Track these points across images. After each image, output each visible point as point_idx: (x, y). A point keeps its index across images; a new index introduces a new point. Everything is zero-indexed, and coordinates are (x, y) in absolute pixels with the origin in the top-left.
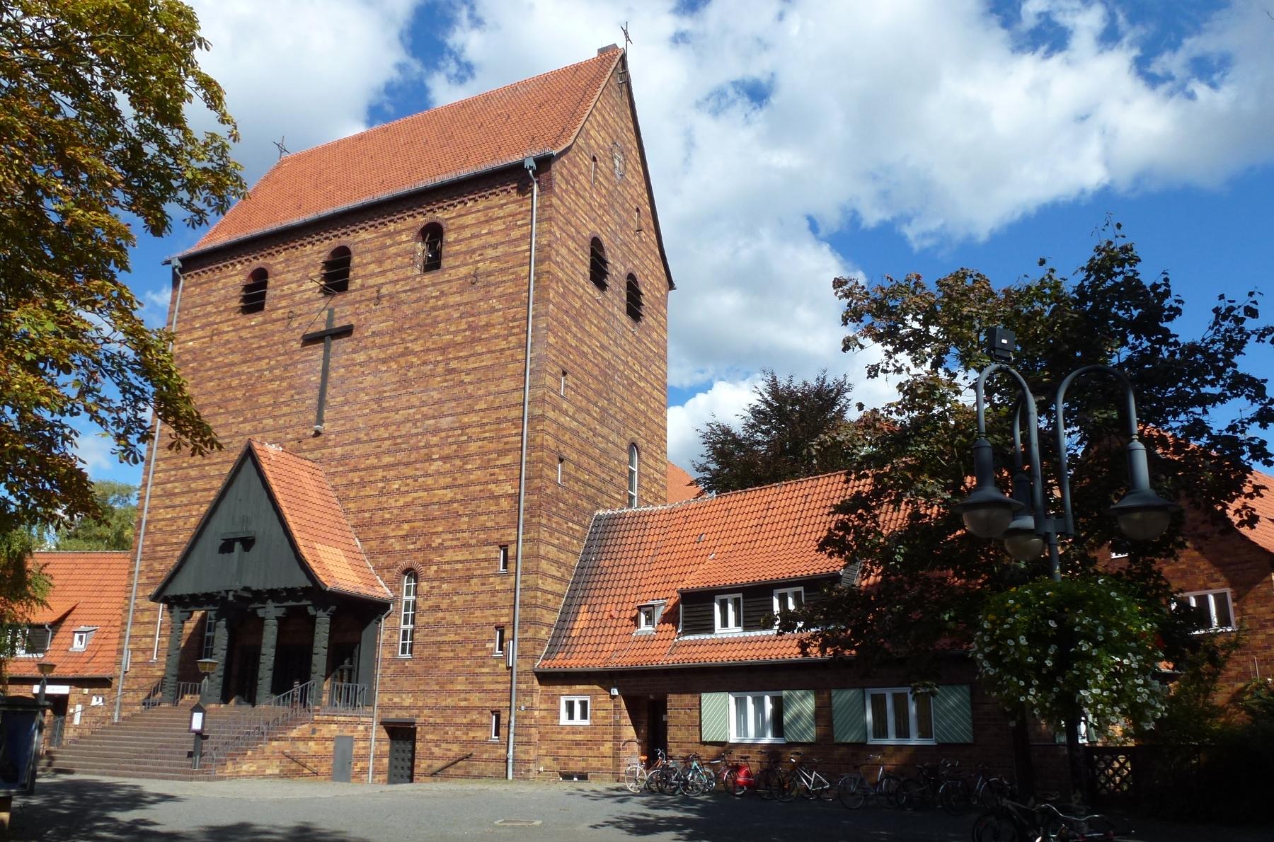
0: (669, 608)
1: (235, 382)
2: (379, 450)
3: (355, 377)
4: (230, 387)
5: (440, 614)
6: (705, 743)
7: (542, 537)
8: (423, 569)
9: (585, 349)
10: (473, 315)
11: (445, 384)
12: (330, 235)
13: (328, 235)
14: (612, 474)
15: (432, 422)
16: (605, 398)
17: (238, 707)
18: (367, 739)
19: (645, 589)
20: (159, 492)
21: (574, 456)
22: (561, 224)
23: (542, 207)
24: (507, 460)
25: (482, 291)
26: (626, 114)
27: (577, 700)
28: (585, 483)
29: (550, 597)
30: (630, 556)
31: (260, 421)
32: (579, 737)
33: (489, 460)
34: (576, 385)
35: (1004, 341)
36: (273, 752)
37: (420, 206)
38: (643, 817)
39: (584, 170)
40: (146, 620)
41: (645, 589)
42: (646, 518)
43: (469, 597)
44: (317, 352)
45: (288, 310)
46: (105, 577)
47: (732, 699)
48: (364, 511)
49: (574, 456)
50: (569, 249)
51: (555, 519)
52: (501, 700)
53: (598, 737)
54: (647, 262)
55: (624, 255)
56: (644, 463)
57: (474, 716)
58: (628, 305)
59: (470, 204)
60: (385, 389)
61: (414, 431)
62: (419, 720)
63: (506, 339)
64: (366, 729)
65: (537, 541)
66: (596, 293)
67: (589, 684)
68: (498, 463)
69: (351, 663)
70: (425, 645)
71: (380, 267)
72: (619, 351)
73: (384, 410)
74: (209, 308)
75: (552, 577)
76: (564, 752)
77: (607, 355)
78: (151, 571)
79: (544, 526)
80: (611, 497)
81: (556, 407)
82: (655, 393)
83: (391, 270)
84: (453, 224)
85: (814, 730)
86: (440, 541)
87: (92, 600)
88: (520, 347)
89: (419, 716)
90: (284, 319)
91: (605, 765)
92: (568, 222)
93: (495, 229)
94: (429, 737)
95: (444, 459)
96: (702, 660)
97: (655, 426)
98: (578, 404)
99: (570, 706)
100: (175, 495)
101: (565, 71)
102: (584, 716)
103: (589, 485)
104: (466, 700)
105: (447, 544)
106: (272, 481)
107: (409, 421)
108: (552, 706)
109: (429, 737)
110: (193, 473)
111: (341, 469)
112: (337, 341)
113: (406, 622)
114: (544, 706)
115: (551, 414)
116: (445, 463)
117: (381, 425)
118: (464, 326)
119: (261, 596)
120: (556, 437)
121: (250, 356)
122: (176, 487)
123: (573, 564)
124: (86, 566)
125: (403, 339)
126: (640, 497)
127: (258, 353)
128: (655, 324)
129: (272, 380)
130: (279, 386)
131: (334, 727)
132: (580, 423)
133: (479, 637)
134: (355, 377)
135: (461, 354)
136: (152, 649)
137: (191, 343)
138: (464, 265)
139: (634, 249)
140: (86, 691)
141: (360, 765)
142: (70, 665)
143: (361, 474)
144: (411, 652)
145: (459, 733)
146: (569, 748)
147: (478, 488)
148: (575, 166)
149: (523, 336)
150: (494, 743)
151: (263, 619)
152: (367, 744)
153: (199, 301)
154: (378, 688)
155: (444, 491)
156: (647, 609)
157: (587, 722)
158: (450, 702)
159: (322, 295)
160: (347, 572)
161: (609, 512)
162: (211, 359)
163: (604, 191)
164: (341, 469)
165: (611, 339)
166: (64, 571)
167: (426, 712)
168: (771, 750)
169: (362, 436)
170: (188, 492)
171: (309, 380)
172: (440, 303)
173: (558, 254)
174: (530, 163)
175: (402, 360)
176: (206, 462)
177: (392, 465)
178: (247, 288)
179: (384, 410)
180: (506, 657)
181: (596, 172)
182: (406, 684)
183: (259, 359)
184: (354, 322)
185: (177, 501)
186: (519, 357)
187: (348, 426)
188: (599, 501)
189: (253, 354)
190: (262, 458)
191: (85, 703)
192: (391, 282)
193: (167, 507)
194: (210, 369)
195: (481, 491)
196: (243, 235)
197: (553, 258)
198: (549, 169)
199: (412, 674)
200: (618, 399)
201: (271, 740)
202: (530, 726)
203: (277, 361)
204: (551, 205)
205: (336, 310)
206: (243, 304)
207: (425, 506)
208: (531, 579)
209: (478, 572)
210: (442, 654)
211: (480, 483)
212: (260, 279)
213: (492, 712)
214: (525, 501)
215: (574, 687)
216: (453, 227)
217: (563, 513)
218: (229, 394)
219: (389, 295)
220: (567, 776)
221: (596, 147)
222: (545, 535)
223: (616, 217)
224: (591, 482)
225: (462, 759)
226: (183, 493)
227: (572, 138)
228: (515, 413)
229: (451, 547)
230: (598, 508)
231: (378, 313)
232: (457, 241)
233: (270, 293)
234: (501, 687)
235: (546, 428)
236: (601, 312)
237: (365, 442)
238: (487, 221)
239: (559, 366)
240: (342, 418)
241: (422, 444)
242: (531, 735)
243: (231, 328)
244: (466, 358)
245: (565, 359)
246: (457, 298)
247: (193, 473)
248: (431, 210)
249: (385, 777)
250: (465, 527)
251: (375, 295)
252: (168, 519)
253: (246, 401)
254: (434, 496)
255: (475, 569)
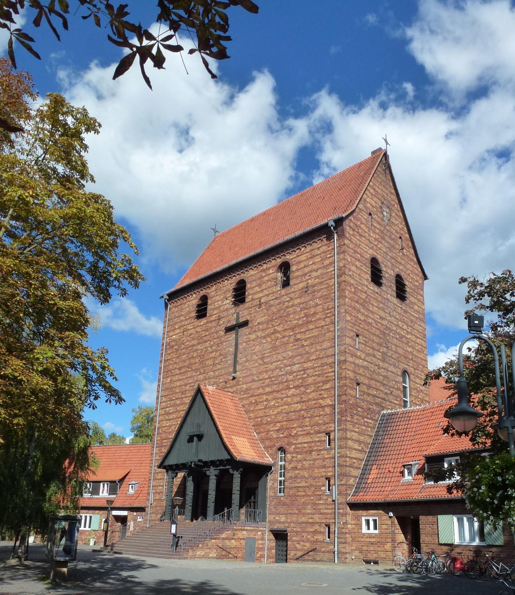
0: (421, 466)
1: (195, 355)
2: (264, 385)
3: (250, 347)
4: (193, 357)
5: (297, 472)
6: (441, 544)
7: (348, 427)
8: (288, 447)
9: (370, 321)
10: (307, 309)
11: (295, 347)
12: (236, 275)
13: (234, 274)
14: (392, 389)
15: (289, 368)
16: (384, 347)
17: (202, 522)
18: (263, 539)
19: (408, 455)
20: (163, 413)
21: (366, 381)
22: (351, 254)
23: (339, 246)
24: (328, 386)
25: (311, 296)
26: (389, 185)
27: (371, 519)
28: (374, 396)
29: (354, 461)
30: (400, 436)
31: (207, 373)
32: (373, 540)
33: (319, 387)
34: (365, 341)
35: (476, 322)
36: (213, 545)
37: (278, 254)
38: (388, 585)
39: (364, 221)
40: (160, 478)
41: (408, 455)
42: (410, 414)
43: (311, 462)
44: (232, 336)
45: (218, 315)
46: (143, 456)
47: (455, 519)
48: (258, 418)
49: (366, 381)
50: (357, 267)
51: (356, 417)
52: (330, 519)
53: (383, 540)
54: (409, 266)
55: (393, 265)
56: (413, 381)
57: (317, 527)
58: (397, 293)
59: (303, 249)
60: (265, 352)
61: (280, 373)
62: (289, 530)
63: (324, 320)
64: (263, 534)
65: (346, 430)
66: (376, 289)
67: (377, 510)
68: (323, 388)
69: (254, 498)
70: (291, 488)
71: (260, 288)
72: (393, 319)
73: (265, 363)
74: (182, 318)
75: (356, 449)
76: (365, 548)
77: (385, 323)
78: (161, 453)
79: (349, 421)
80: (391, 402)
81: (353, 355)
82: (418, 341)
83: (265, 289)
84: (294, 261)
85: (502, 537)
86: (295, 432)
87: (137, 468)
88: (332, 323)
89: (289, 527)
90: (216, 320)
91: (388, 556)
92: (356, 252)
93: (316, 261)
94: (294, 538)
95: (295, 387)
96: (437, 496)
97: (419, 360)
98: (368, 352)
99: (368, 522)
100: (170, 413)
101: (354, 167)
102: (375, 528)
103: (377, 397)
104: (312, 518)
105: (299, 433)
106: (210, 405)
107: (278, 368)
108: (358, 522)
109: (294, 538)
110: (178, 402)
111: (246, 396)
112: (241, 329)
113: (281, 476)
114: (353, 522)
115: (350, 359)
116: (296, 390)
117: (264, 372)
118: (303, 315)
119: (207, 464)
120: (354, 372)
121: (201, 340)
122: (170, 410)
123: (368, 442)
124: (134, 451)
125: (273, 325)
126: (411, 402)
127: (205, 338)
128: (416, 301)
129: (212, 352)
130: (215, 355)
131: (245, 532)
132: (369, 362)
133: (317, 484)
134: (250, 347)
135: (302, 330)
136: (162, 492)
137: (174, 336)
138: (301, 282)
139: (399, 259)
140: (135, 513)
141: (260, 553)
142: (128, 501)
143: (256, 398)
144: (284, 492)
145: (309, 537)
146: (367, 546)
147: (313, 402)
148: (358, 220)
149: (333, 317)
150: (327, 543)
151: (209, 476)
152: (263, 542)
153: (177, 315)
154: (267, 512)
155: (296, 405)
156: (408, 467)
157: (377, 532)
158: (304, 519)
159: (233, 306)
160: (249, 450)
161: (389, 411)
162: (183, 344)
163: (377, 231)
164: (246, 396)
165: (386, 313)
166: (124, 454)
167: (292, 525)
168: (478, 551)
169: (255, 378)
170: (176, 412)
171: (229, 351)
172: (290, 304)
173: (350, 270)
174: (332, 223)
175: (273, 336)
176: (183, 396)
177: (270, 393)
178: (199, 306)
179: (265, 363)
180: (331, 495)
181: (372, 221)
182: (282, 509)
183: (205, 342)
184: (249, 318)
185: (171, 417)
186: (332, 329)
187: (248, 373)
188: (384, 405)
189: (203, 339)
190: (205, 393)
191: (135, 520)
192: (266, 295)
193: (167, 420)
194: (183, 349)
195: (315, 404)
196: (195, 279)
197: (347, 273)
198: (342, 224)
199: (285, 504)
200: (393, 346)
201: (211, 539)
202: (346, 533)
203: (214, 342)
204: (344, 244)
205: (240, 313)
206: (197, 314)
207: (287, 413)
208: (343, 451)
209: (315, 448)
210: (299, 493)
211: (314, 400)
212: (204, 300)
213: (326, 525)
214: (338, 408)
215: (369, 512)
216: (295, 263)
217: (361, 414)
218: (193, 361)
219: (265, 302)
220: (368, 562)
221: (371, 207)
222: (349, 426)
223: (386, 244)
224: (378, 395)
225: (311, 551)
226: (174, 412)
227: (355, 206)
228: (331, 360)
229: (301, 435)
230: (383, 409)
231: (260, 313)
232: (297, 270)
233: (209, 307)
234: (330, 511)
235: (347, 367)
236: (380, 299)
237: (257, 381)
238: (312, 257)
239: (354, 332)
240: (245, 369)
241: (284, 380)
242: (346, 538)
243: (192, 327)
244: (304, 332)
245: (357, 328)
246: (299, 301)
247: (178, 402)
248: (284, 255)
249: (274, 560)
250: (308, 424)
251: (259, 303)
252: (167, 426)
253: (200, 364)
254: (292, 408)
255: (314, 447)
